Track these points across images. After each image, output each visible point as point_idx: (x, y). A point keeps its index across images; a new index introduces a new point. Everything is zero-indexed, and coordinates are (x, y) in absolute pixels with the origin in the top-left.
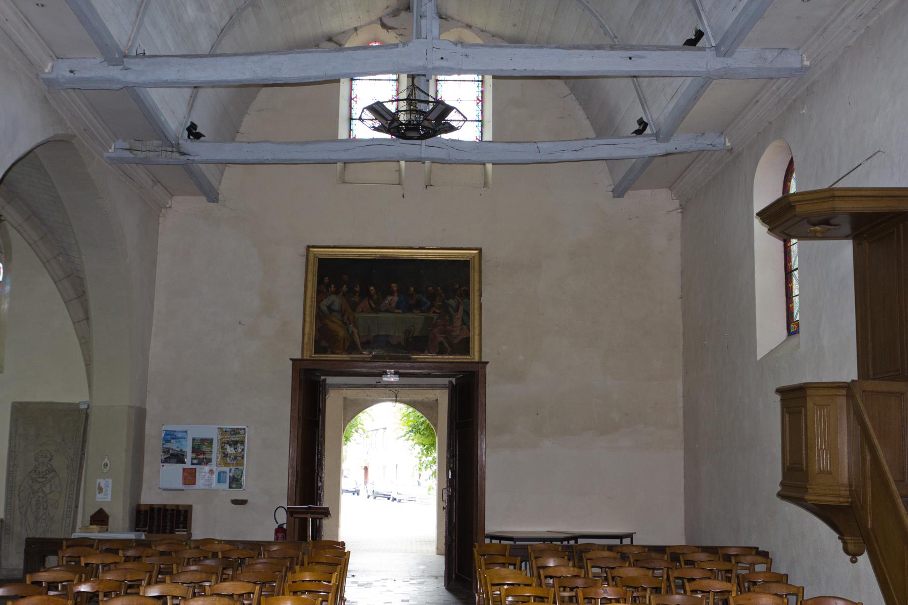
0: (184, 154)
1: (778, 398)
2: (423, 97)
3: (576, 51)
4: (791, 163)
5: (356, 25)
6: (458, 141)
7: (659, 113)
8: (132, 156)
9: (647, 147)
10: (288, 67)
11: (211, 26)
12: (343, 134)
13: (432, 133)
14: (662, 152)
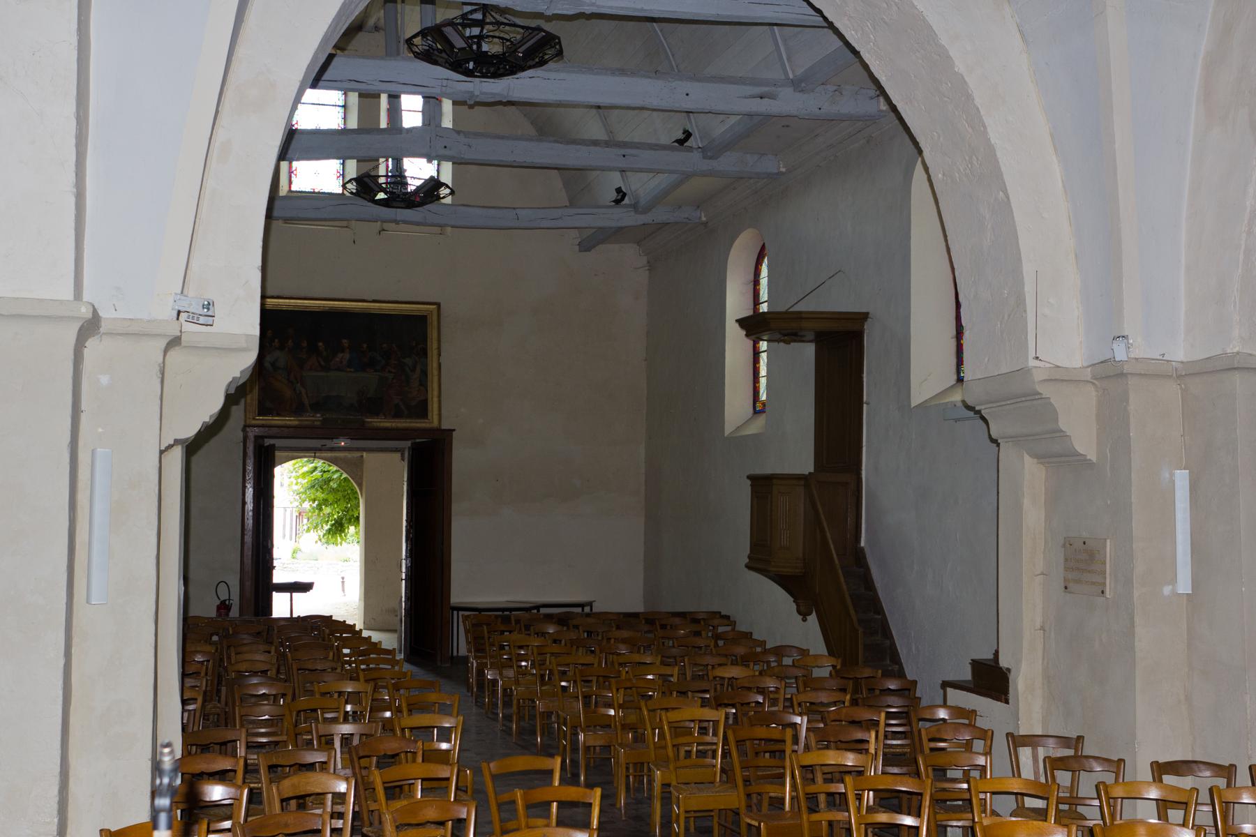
1: (749, 482)
4: (763, 247)
7: (642, 186)
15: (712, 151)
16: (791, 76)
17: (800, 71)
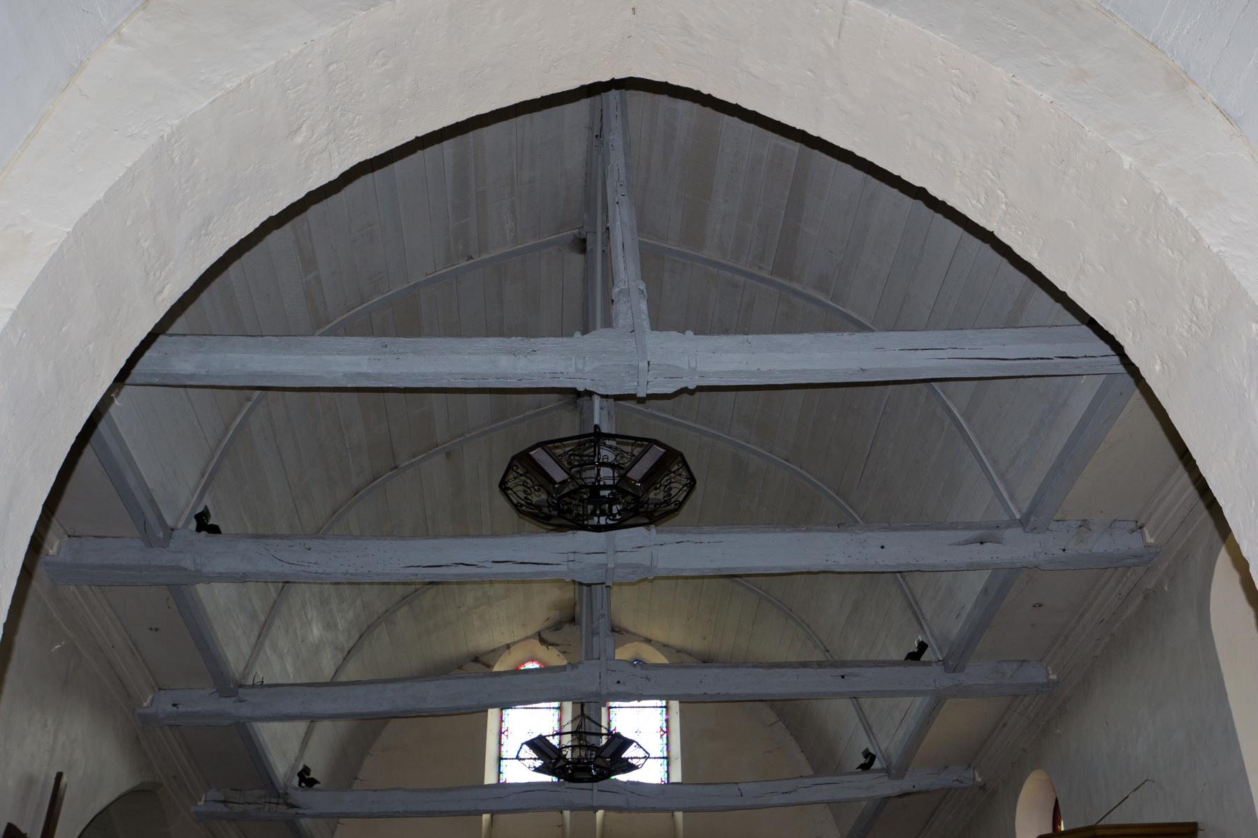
0: (292, 806)
2: (594, 729)
3: (777, 670)
4: (1057, 801)
5: (508, 641)
6: (638, 783)
8: (226, 810)
9: (878, 786)
10: (433, 694)
11: (336, 648)
12: (490, 779)
13: (606, 773)
14: (897, 791)
15: (954, 661)
16: (1018, 517)
17: (1025, 506)
